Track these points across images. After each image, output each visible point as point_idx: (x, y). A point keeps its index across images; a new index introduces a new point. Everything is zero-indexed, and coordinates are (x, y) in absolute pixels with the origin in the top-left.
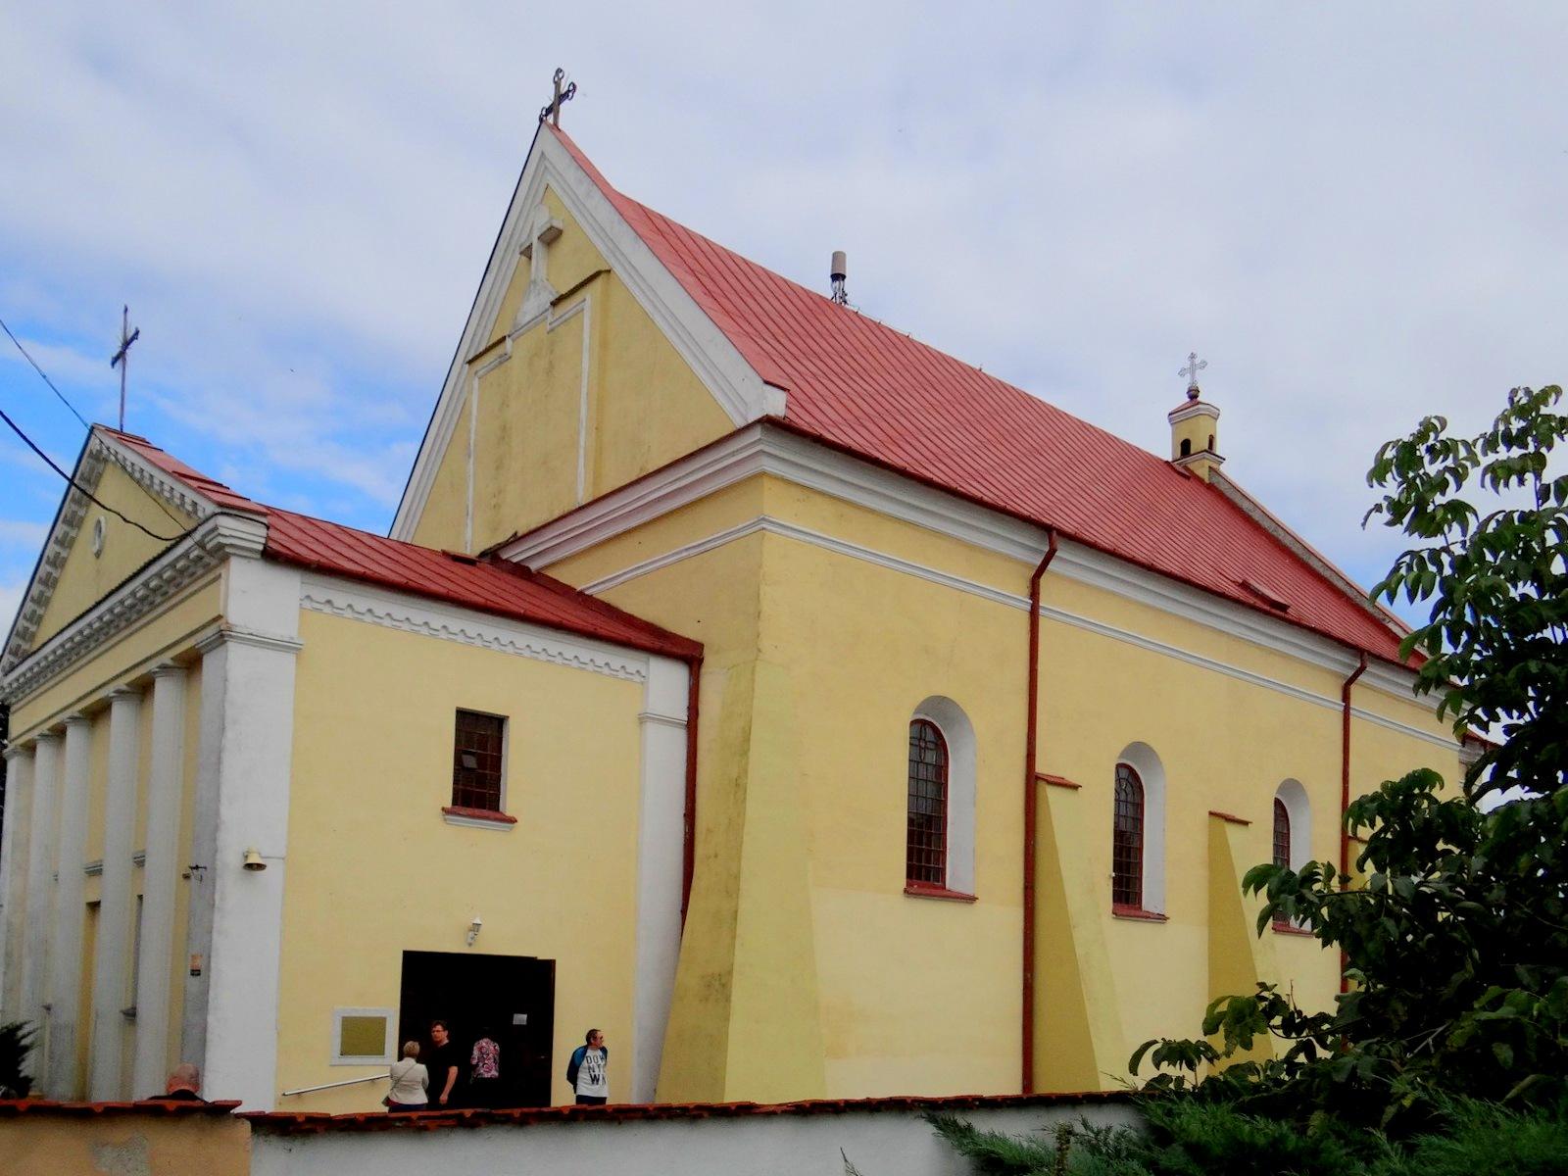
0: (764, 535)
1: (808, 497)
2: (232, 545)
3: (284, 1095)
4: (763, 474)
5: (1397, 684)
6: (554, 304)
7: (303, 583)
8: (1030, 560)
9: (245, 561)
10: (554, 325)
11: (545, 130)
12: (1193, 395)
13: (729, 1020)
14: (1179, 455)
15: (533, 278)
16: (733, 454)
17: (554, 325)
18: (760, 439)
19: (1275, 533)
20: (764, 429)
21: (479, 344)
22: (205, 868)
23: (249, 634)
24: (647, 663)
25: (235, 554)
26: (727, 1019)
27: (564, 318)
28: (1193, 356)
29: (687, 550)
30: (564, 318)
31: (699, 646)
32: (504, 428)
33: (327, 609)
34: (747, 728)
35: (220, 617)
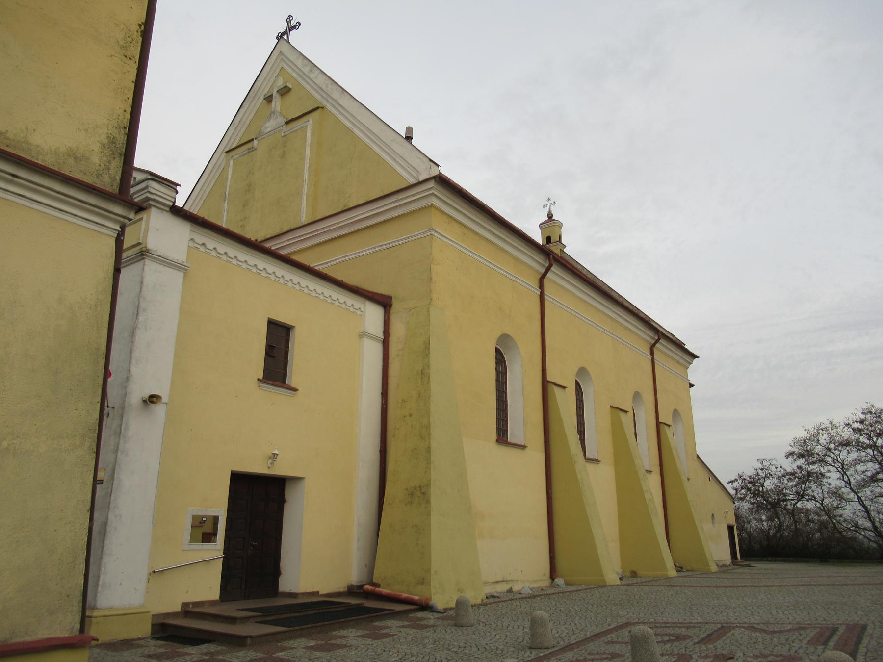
0: (432, 238)
1: (450, 222)
2: (154, 200)
3: (154, 572)
4: (432, 206)
5: (669, 349)
6: (287, 123)
7: (191, 230)
8: (540, 270)
9: (160, 211)
10: (287, 133)
11: (282, 41)
12: (550, 216)
13: (430, 515)
14: (545, 243)
15: (273, 110)
16: (414, 195)
17: (287, 133)
18: (433, 187)
19: (594, 280)
20: (436, 181)
21: (233, 143)
22: (113, 407)
23: (158, 256)
24: (364, 304)
25: (154, 206)
26: (429, 514)
27: (293, 130)
28: (549, 200)
29: (380, 246)
30: (293, 130)
31: (390, 298)
32: (250, 185)
33: (202, 249)
34: (427, 342)
35: (139, 244)
